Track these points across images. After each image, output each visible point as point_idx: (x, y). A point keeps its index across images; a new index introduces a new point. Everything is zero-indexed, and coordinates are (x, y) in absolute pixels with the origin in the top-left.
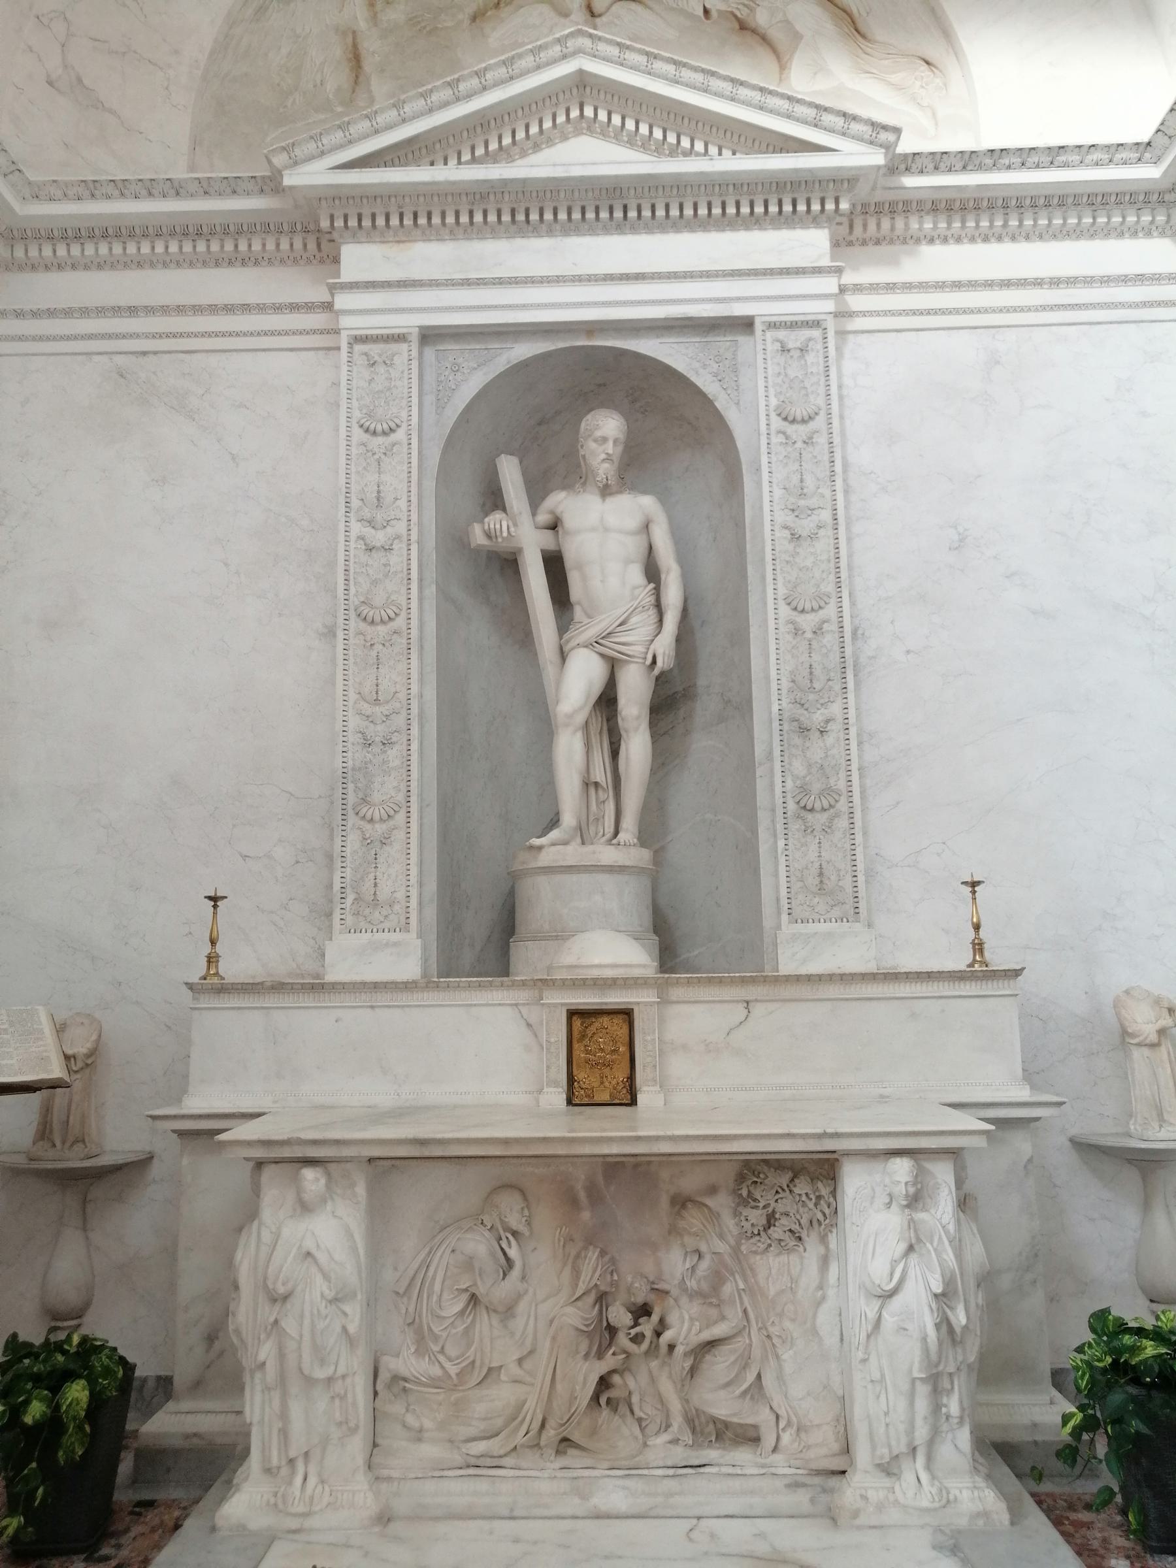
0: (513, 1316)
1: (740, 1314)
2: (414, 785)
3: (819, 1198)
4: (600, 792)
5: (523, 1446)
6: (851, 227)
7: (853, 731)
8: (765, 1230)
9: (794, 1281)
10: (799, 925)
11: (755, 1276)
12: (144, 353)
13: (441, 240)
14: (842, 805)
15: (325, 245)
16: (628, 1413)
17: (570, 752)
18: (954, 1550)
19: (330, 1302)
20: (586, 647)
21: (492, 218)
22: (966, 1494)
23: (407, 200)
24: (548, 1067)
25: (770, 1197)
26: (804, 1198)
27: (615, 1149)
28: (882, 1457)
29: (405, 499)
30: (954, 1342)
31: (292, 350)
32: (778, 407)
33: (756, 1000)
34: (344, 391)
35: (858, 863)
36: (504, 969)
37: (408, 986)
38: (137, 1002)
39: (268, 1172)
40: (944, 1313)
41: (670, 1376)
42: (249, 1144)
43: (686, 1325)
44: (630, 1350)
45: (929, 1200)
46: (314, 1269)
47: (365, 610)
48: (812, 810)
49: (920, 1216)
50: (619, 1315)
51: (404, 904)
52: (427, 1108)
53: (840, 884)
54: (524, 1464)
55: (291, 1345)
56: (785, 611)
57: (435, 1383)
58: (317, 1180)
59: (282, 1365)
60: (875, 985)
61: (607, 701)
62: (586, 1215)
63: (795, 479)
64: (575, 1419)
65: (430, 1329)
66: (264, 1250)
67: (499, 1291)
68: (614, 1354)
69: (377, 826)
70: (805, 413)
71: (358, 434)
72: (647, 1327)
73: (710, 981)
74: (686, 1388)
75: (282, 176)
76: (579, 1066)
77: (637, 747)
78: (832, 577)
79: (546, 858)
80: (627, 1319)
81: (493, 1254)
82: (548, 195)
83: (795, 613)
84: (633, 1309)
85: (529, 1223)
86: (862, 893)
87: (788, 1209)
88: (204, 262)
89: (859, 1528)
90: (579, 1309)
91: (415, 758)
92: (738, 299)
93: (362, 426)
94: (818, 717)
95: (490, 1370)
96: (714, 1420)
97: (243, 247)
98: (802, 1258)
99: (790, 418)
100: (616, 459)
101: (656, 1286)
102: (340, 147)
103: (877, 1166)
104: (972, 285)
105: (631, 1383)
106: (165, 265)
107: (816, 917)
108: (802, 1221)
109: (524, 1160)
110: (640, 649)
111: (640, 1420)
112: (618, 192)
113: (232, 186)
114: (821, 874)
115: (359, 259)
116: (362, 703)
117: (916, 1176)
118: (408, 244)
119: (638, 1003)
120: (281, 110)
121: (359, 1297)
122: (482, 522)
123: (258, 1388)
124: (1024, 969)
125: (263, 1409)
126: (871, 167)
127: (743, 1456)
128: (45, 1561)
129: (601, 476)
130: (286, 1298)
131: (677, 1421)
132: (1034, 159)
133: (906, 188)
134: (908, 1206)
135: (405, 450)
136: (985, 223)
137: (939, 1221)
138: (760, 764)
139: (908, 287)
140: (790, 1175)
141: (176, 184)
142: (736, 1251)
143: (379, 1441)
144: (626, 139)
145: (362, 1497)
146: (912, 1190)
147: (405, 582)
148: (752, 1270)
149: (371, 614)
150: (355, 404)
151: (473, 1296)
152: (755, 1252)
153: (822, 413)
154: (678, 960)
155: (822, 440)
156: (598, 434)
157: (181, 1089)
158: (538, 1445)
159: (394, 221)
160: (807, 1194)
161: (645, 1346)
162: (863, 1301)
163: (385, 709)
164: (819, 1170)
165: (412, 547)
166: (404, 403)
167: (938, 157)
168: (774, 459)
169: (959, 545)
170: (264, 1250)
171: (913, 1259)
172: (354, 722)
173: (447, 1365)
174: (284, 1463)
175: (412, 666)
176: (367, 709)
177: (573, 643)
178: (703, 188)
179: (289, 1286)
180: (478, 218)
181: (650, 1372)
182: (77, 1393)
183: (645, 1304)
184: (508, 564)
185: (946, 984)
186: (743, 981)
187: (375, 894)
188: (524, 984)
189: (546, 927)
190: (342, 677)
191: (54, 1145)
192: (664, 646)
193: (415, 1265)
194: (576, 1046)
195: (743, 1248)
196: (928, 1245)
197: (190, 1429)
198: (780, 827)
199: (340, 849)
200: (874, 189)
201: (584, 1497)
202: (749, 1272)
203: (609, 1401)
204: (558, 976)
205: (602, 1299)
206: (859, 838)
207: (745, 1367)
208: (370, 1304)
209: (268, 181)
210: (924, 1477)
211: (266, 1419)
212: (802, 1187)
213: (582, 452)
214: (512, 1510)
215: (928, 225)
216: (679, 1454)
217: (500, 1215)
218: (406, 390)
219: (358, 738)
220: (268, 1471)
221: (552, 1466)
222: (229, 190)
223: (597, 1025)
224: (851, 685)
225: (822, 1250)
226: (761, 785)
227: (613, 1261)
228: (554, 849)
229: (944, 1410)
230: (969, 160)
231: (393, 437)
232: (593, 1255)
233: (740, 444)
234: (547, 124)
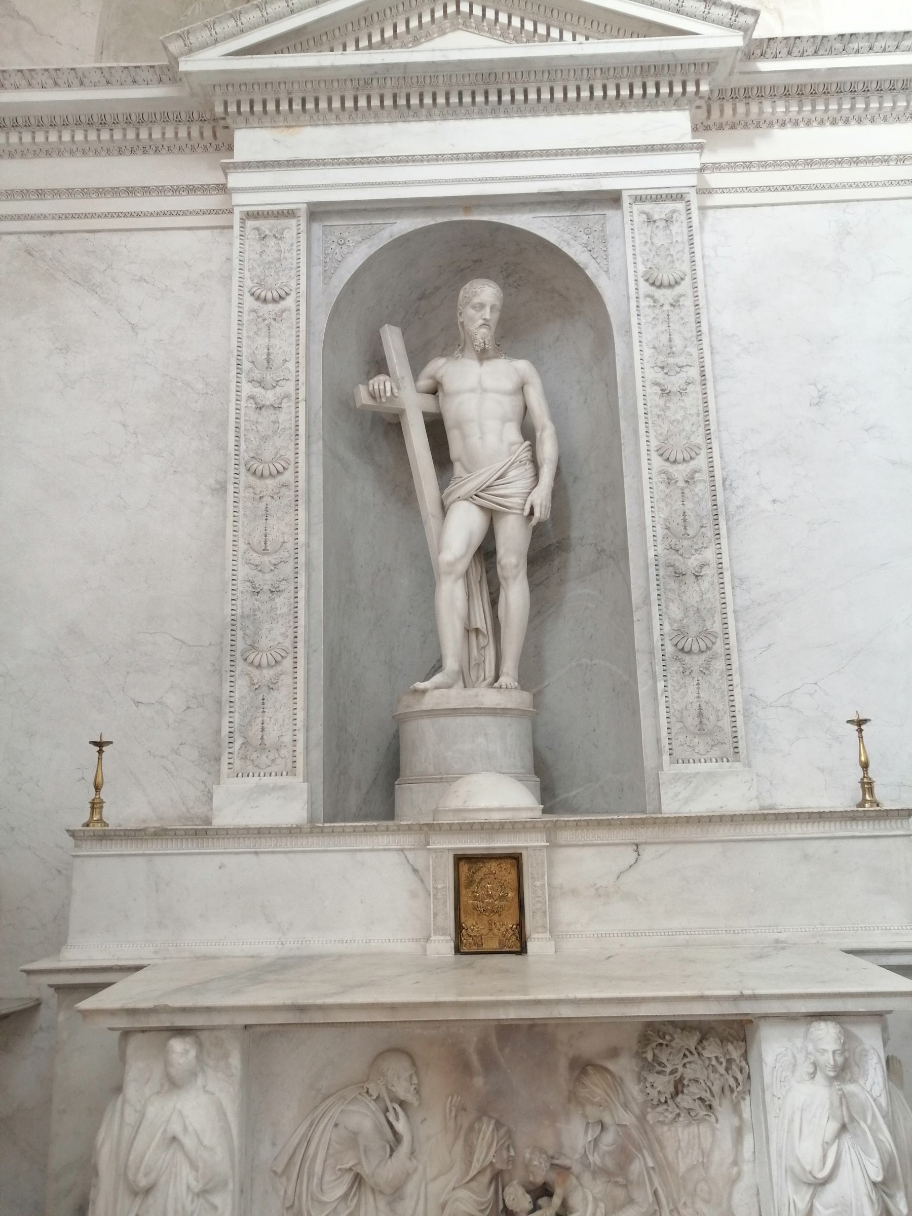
0: (401, 1198)
1: (651, 1198)
2: (301, 631)
3: (730, 1061)
4: (481, 637)
6: (709, 112)
7: (727, 576)
8: (672, 1097)
9: (706, 1154)
10: (681, 765)
11: (662, 1147)
12: (52, 233)
13: (328, 124)
14: (719, 647)
15: (220, 132)
17: (452, 598)
19: (198, 1195)
20: (466, 500)
21: (375, 102)
23: (296, 86)
24: (435, 914)
25: (678, 1061)
26: (714, 1062)
27: (512, 1014)
29: (293, 361)
31: (189, 229)
32: (646, 273)
33: (646, 843)
34: (236, 262)
35: (736, 703)
36: (389, 813)
37: (292, 832)
39: (134, 1042)
40: (884, 1202)
42: (112, 1013)
45: (856, 1069)
46: (180, 1156)
47: (255, 465)
48: (690, 652)
49: (850, 1088)
51: (291, 748)
52: (310, 959)
53: (720, 724)
56: (657, 462)
58: (186, 1052)
60: (766, 826)
61: (486, 552)
62: (479, 1081)
63: (664, 339)
66: (127, 1132)
67: (386, 1171)
69: (265, 671)
70: (671, 278)
71: (249, 302)
73: (599, 823)
75: (178, 64)
76: (466, 912)
77: (516, 595)
78: (701, 430)
79: (430, 702)
81: (378, 1130)
82: (428, 80)
83: (667, 464)
85: (417, 1091)
86: (741, 733)
87: (698, 1075)
88: (108, 150)
90: (473, 1192)
91: (301, 605)
92: (606, 175)
93: (253, 295)
94: (693, 562)
97: (144, 135)
98: (713, 1130)
99: (658, 283)
100: (493, 324)
101: (556, 1162)
102: (233, 36)
103: (799, 1030)
104: (824, 162)
106: (72, 153)
107: (697, 757)
108: (713, 1089)
110: (518, 501)
112: (493, 78)
113: (132, 76)
114: (700, 715)
115: (249, 142)
116: (252, 553)
118: (297, 129)
119: (527, 848)
120: (182, 18)
121: (231, 1186)
122: (368, 385)
126: (731, 49)
129: (479, 340)
130: (148, 1191)
132: (881, 43)
133: (764, 72)
134: (836, 1078)
135: (294, 316)
136: (833, 106)
137: (870, 1092)
138: (637, 608)
139: (764, 165)
140: (696, 1037)
141: (80, 74)
144: (499, 32)
146: (840, 1060)
147: (293, 438)
148: (660, 1142)
149: (261, 467)
150: (247, 274)
152: (662, 1123)
153: (688, 279)
154: (557, 800)
155: (688, 302)
156: (476, 300)
157: (59, 942)
159: (284, 106)
160: (717, 1058)
162: (790, 1188)
163: (273, 559)
164: (734, 1032)
165: (300, 405)
166: (293, 273)
167: (792, 41)
168: (643, 321)
169: (819, 401)
170: (127, 1132)
171: (847, 1141)
172: (243, 571)
175: (299, 517)
176: (255, 558)
177: (454, 496)
178: (572, 73)
179: (153, 1175)
180: (362, 103)
183: (545, 1183)
184: (392, 426)
185: (838, 824)
186: (632, 823)
187: (262, 738)
188: (409, 828)
189: (431, 769)
190: (232, 528)
192: (541, 497)
194: (463, 892)
195: (649, 1117)
196: (862, 1123)
198: (659, 669)
199: (228, 694)
200: (731, 73)
202: (656, 1147)
204: (445, 820)
205: (498, 1178)
206: (736, 679)
209: (166, 71)
212: (711, 1050)
213: (460, 319)
215: (781, 109)
218: (295, 262)
219: (247, 586)
222: (129, 80)
223: (485, 870)
224: (723, 531)
225: (736, 1121)
226: (638, 629)
227: (509, 1132)
228: (438, 693)
230: (820, 45)
231: (283, 304)
232: (487, 1129)
233: (610, 309)
234: (426, 19)
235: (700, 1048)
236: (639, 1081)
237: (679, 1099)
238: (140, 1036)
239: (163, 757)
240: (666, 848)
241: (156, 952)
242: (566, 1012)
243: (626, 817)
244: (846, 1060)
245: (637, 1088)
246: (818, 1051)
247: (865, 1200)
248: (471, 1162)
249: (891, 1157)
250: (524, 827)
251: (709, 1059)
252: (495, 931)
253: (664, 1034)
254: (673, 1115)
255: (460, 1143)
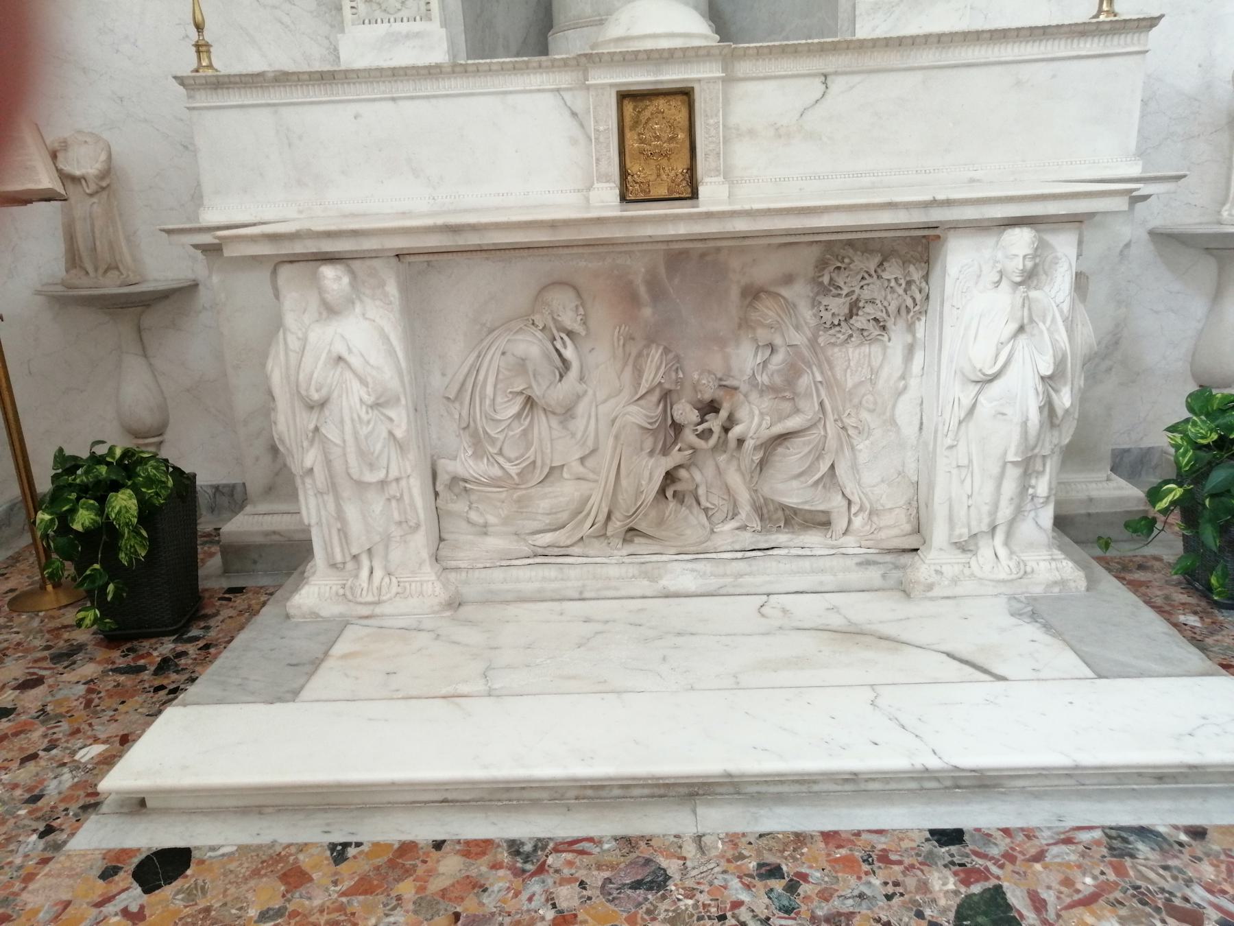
1: (817, 407)
3: (909, 283)
5: (589, 536)
9: (875, 372)
11: (831, 368)
16: (695, 503)
18: (1034, 616)
19: (371, 407)
22: (1043, 565)
24: (598, 160)
25: (855, 283)
26: (893, 284)
28: (961, 536)
30: (1053, 425)
33: (836, 73)
36: (544, 51)
37: (432, 72)
38: (145, 121)
40: (1049, 396)
41: (739, 469)
43: (756, 420)
44: (696, 446)
45: (1044, 277)
46: (348, 375)
49: (1033, 294)
50: (685, 412)
54: (591, 552)
55: (336, 452)
57: (495, 482)
58: (340, 278)
59: (329, 471)
62: (647, 312)
64: (642, 510)
65: (486, 432)
68: (680, 450)
72: (715, 423)
74: (755, 479)
80: (694, 416)
84: (700, 406)
85: (584, 322)
87: (875, 295)
89: (932, 599)
95: (552, 469)
96: (783, 507)
98: (885, 348)
105: (698, 477)
108: (890, 309)
109: (575, 250)
111: (706, 510)
117: (1036, 249)
119: (699, 80)
121: (403, 402)
123: (311, 492)
124: (1162, 16)
125: (319, 511)
127: (813, 539)
128: (135, 643)
130: (323, 404)
131: (745, 509)
140: (877, 259)
142: (813, 342)
143: (444, 536)
145: (429, 587)
146: (1029, 264)
151: (529, 398)
152: (833, 344)
158: (604, 535)
160: (896, 279)
161: (713, 441)
171: (1022, 338)
173: (507, 466)
174: (348, 558)
179: (324, 392)
181: (718, 467)
182: (124, 502)
191: (87, 273)
193: (465, 370)
194: (628, 134)
195: (820, 340)
196: (1041, 324)
197: (266, 528)
201: (653, 579)
202: (826, 366)
203: (675, 494)
205: (666, 397)
207: (819, 457)
208: (419, 409)
210: (1002, 552)
211: (324, 520)
212: (892, 271)
214: (581, 593)
216: (747, 539)
217: (551, 313)
220: (334, 566)
221: (620, 553)
223: (652, 108)
227: (678, 358)
229: (1031, 491)
232: (656, 353)
235: (879, 270)
236: (813, 306)
237: (852, 321)
238: (288, 267)
239: (274, 7)
240: (856, 79)
241: (300, 212)
242: (741, 226)
243: (816, 41)
244: (1036, 265)
245: (810, 312)
246: (1007, 257)
247: (1032, 393)
248: (639, 384)
249: (1064, 356)
250: (697, 56)
251: (889, 280)
252: (664, 177)
253: (843, 258)
254: (846, 336)
255: (629, 369)
